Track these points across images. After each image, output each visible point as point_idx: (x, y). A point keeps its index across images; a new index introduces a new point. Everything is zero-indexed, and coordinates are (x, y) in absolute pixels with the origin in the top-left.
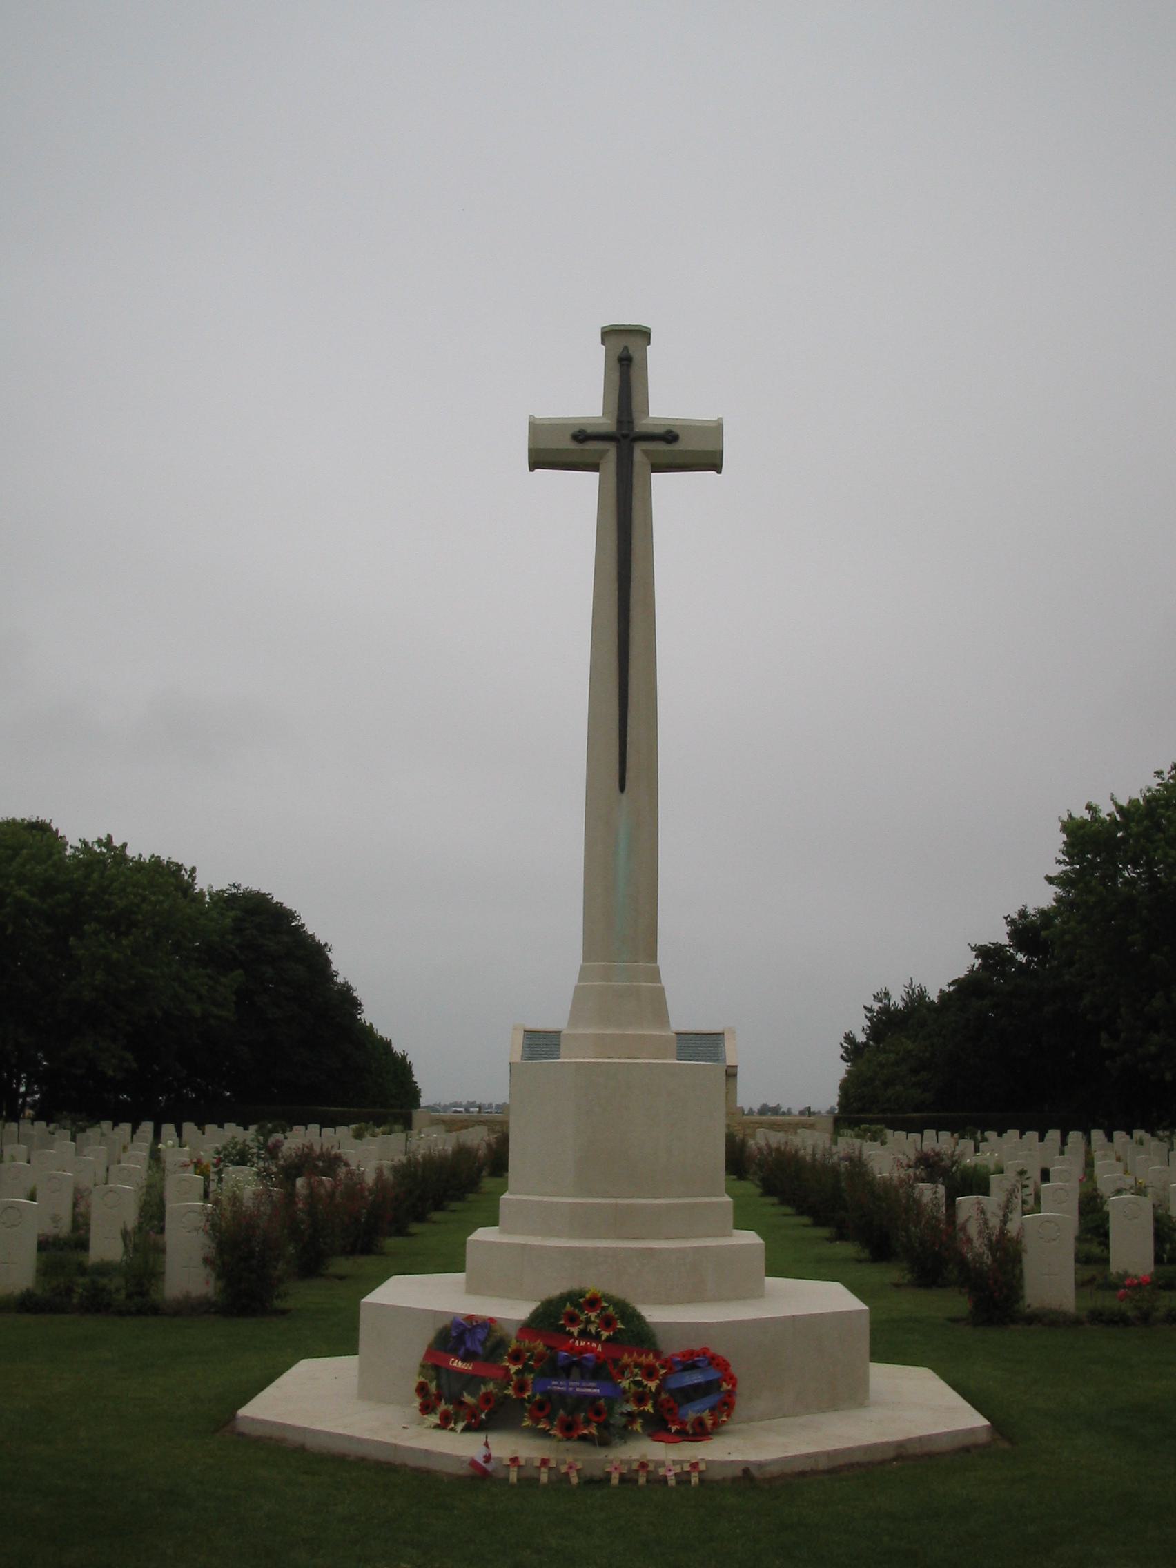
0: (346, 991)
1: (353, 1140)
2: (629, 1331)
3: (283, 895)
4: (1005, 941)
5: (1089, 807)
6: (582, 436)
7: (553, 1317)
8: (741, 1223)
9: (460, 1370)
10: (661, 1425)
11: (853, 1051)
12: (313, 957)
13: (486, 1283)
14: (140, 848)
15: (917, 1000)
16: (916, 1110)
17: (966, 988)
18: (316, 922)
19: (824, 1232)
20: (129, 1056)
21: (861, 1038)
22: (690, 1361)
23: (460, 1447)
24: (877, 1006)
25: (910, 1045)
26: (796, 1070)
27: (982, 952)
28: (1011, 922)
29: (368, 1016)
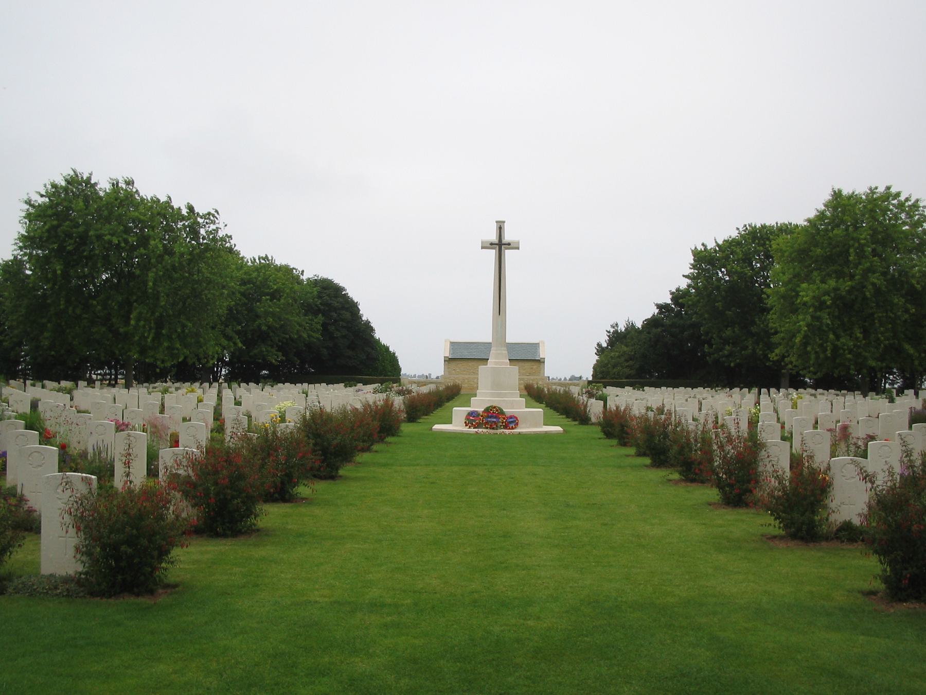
0: (368, 323)
1: (458, 382)
2: (500, 412)
3: (338, 280)
4: (670, 302)
5: (703, 245)
6: (492, 244)
7: (487, 410)
8: (521, 396)
9: (472, 419)
10: (506, 427)
11: (600, 350)
12: (352, 308)
13: (478, 404)
14: (279, 261)
15: (631, 328)
16: (626, 378)
17: (651, 323)
18: (354, 292)
19: (576, 423)
20: (280, 354)
21: (605, 345)
22: (511, 417)
23: (473, 430)
24: (612, 330)
25: (625, 349)
26: (571, 360)
27: (659, 306)
28: (672, 293)
29: (377, 335)
